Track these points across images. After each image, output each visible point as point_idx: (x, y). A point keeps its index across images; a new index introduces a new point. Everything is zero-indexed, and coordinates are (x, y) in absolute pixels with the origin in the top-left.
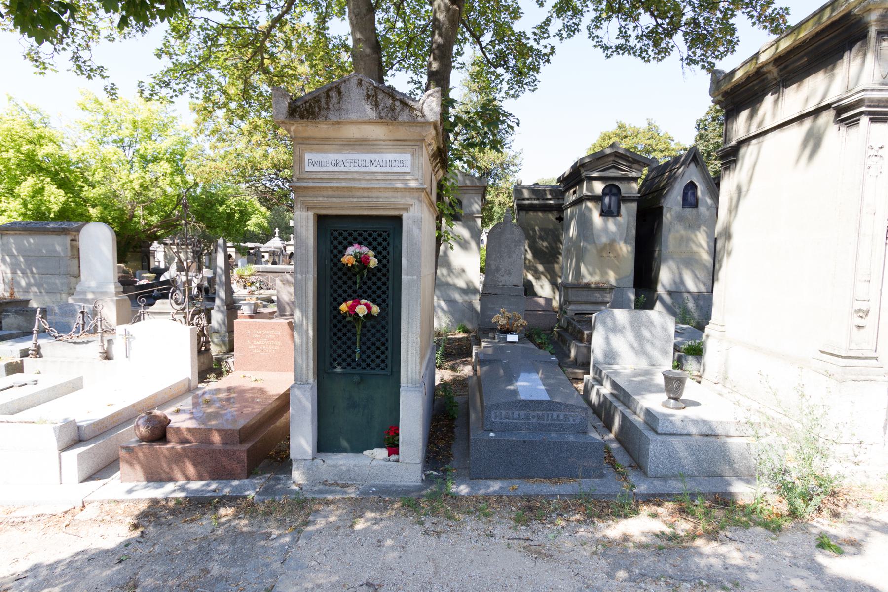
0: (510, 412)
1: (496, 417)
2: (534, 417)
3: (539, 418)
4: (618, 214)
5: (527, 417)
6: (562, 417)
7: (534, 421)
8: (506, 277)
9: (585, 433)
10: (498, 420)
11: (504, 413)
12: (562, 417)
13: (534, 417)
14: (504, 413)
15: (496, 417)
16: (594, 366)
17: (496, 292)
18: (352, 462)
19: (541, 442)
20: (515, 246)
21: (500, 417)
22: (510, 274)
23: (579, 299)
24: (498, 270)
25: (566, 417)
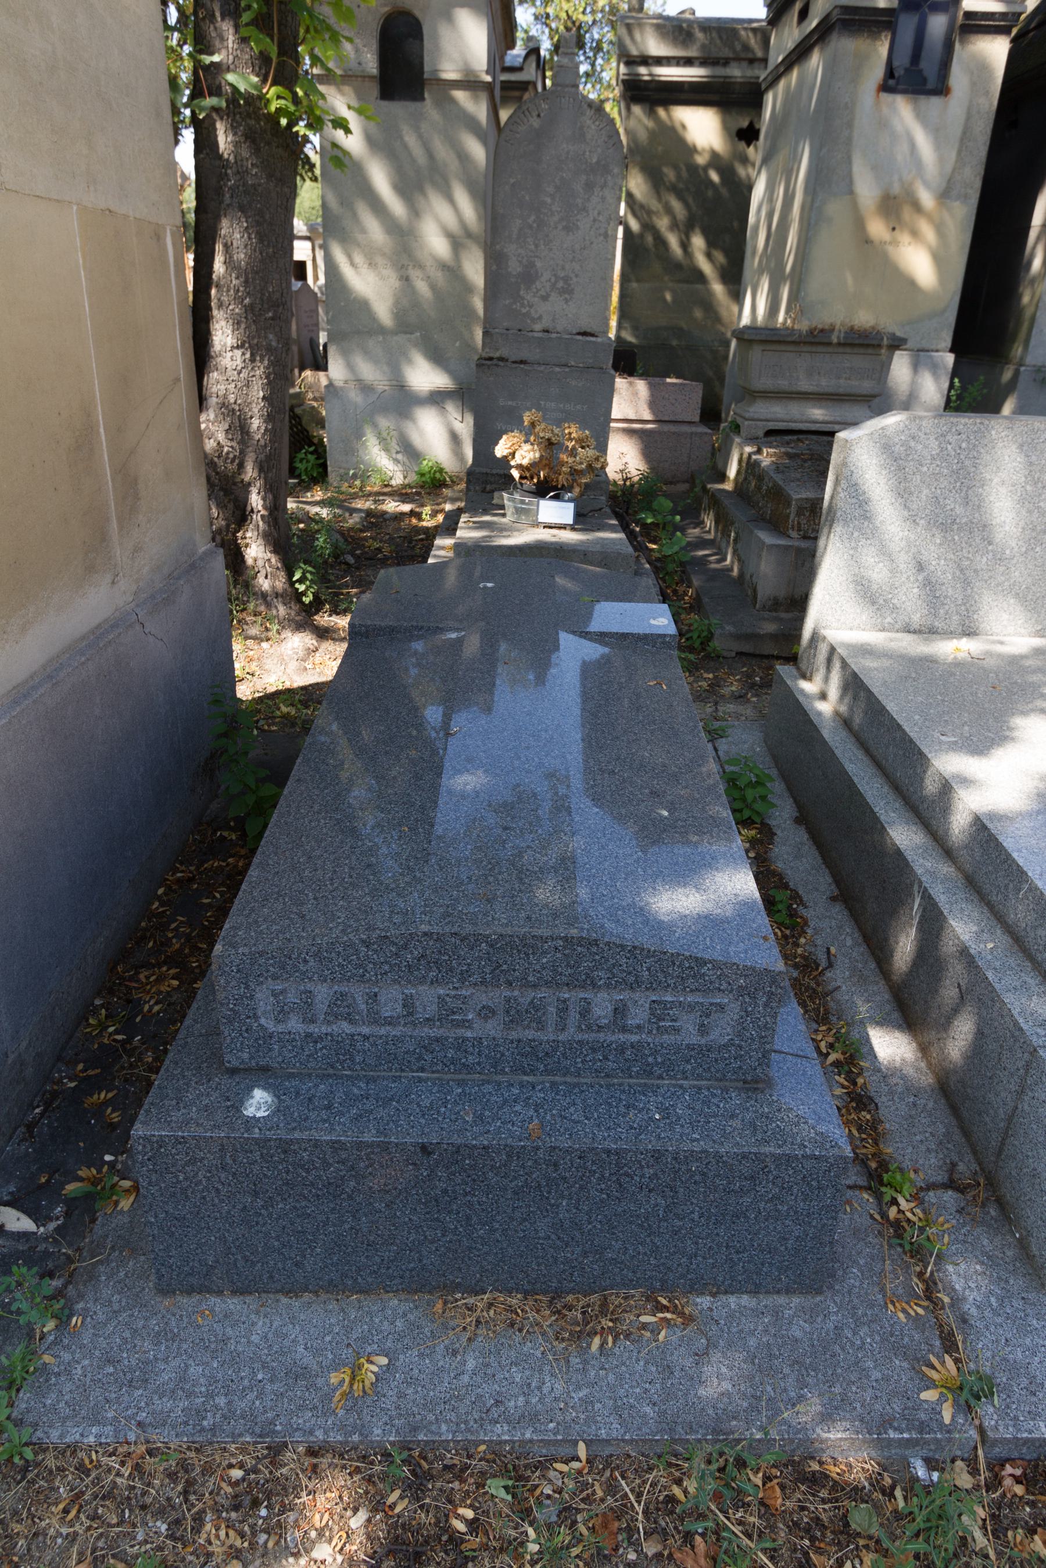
0: (358, 993)
1: (282, 1014)
2: (487, 1013)
3: (514, 1016)
4: (942, 89)
5: (447, 1014)
6: (638, 1015)
7: (492, 1028)
8: (556, 303)
9: (756, 1085)
10: (295, 1024)
11: (323, 993)
12: (638, 1015)
13: (487, 1013)
14: (323, 993)
15: (282, 1014)
16: (937, 1255)
17: (524, 355)
18: (855, 383)
19: (512, 1153)
20: (589, 186)
21: (306, 1007)
22: (567, 291)
23: (783, 384)
24: (529, 277)
25: (659, 1013)
